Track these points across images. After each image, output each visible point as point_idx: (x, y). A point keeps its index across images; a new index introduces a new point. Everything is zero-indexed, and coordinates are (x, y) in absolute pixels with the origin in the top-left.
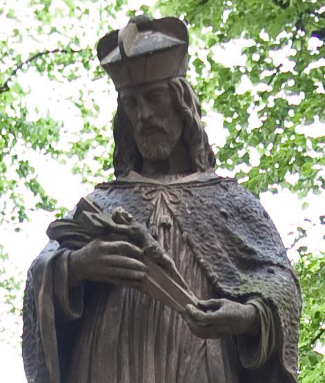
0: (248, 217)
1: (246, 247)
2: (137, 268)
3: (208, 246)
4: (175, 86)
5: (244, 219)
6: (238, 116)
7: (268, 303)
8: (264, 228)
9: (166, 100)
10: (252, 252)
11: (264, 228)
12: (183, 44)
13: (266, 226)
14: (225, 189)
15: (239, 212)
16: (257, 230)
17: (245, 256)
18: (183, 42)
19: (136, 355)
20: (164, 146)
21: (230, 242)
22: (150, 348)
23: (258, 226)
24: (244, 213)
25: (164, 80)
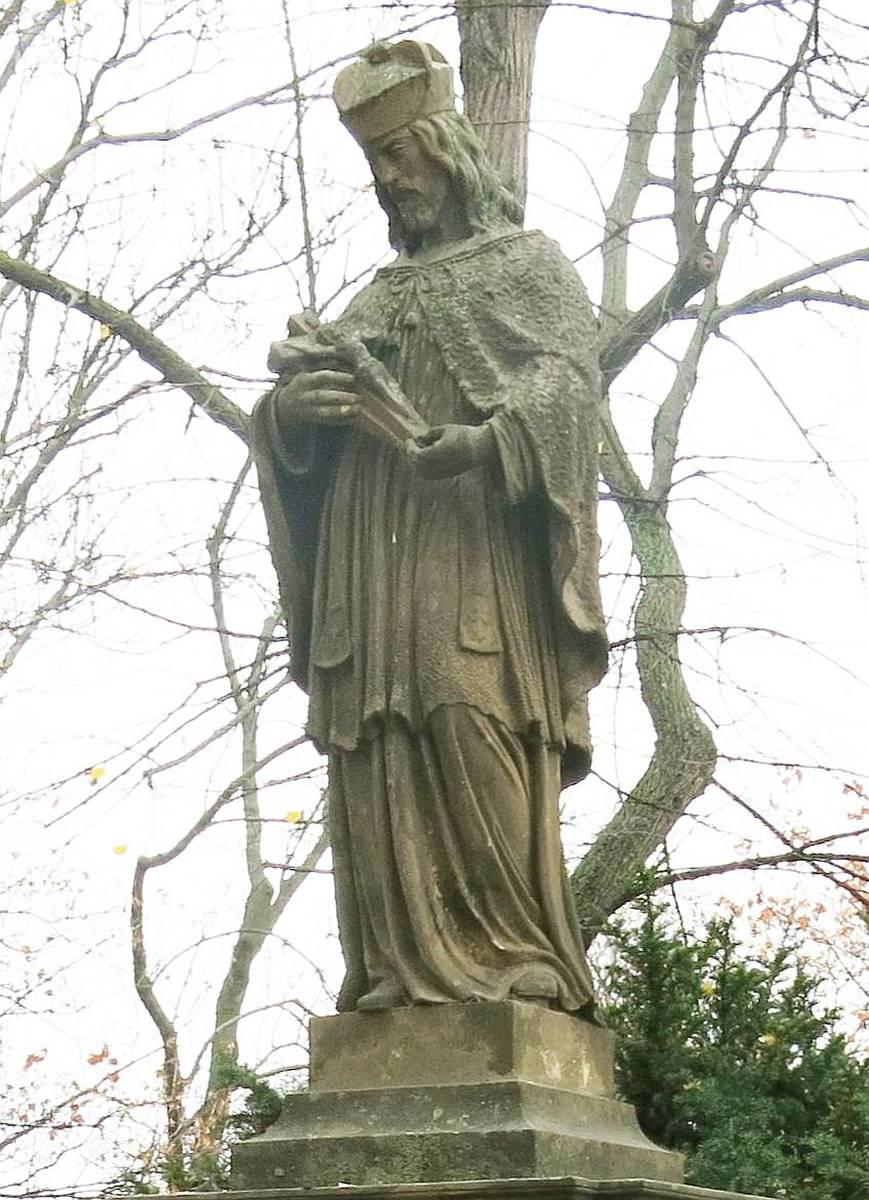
0: (531, 287)
1: (514, 334)
2: (338, 403)
3: (460, 345)
4: (420, 133)
5: (525, 291)
6: (26, 259)
7: (515, 417)
8: (550, 299)
9: (411, 152)
10: (521, 340)
11: (550, 299)
12: (420, 76)
13: (551, 295)
14: (503, 252)
15: (519, 283)
16: (542, 304)
17: (513, 347)
18: (420, 71)
19: (366, 515)
20: (423, 212)
21: (493, 332)
22: (378, 500)
23: (542, 298)
24: (526, 282)
25: (403, 126)
